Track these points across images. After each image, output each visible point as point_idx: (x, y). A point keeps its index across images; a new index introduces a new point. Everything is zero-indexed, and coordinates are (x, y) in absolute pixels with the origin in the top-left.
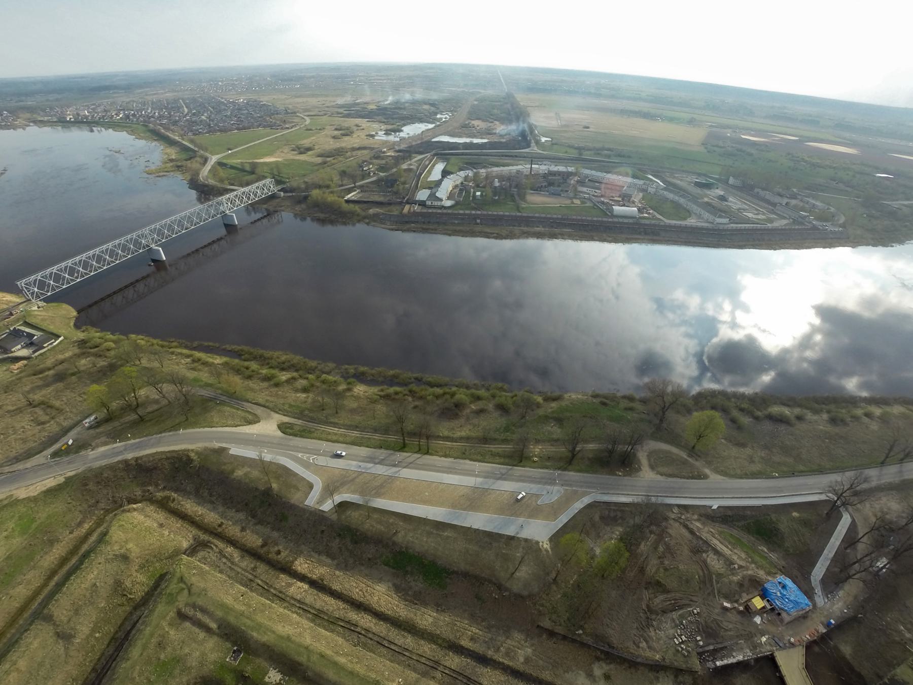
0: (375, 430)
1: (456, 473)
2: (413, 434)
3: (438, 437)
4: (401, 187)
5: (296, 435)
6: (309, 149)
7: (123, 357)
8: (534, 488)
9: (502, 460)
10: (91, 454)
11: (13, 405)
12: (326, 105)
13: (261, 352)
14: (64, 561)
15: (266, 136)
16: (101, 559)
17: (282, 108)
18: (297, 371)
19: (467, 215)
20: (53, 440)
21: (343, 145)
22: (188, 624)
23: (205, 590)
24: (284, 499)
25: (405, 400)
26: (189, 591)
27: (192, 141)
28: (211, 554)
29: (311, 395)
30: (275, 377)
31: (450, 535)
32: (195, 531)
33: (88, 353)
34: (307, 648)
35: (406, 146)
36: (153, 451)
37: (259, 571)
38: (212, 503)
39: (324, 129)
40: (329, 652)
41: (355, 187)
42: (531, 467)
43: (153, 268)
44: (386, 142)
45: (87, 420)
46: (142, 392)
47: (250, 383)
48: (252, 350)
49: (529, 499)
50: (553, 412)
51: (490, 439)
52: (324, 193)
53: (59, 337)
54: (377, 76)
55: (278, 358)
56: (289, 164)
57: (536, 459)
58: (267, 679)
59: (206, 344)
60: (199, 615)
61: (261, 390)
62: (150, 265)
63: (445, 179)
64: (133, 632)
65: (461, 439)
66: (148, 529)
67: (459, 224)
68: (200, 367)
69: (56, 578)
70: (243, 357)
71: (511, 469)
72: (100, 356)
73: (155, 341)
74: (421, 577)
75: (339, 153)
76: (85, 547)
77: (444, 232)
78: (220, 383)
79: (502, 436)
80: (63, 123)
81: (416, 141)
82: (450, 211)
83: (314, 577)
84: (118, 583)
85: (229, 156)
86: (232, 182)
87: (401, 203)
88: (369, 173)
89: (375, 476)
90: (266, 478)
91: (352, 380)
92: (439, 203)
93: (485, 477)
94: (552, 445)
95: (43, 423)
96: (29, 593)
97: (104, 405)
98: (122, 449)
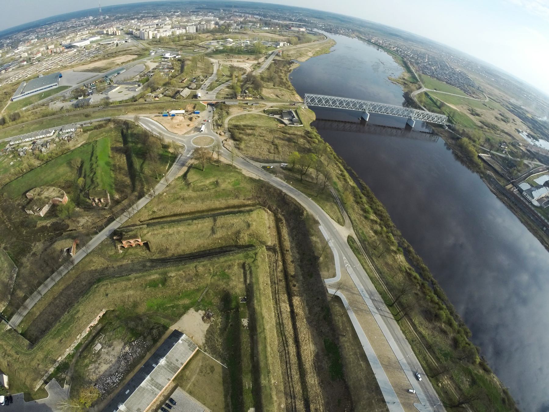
0: (387, 284)
1: (398, 345)
2: (401, 304)
3: (410, 320)
4: (515, 172)
5: (351, 248)
6: (478, 115)
7: (317, 150)
8: (422, 396)
9: (425, 366)
10: (274, 177)
11: (268, 139)
12: (503, 98)
13: (373, 196)
14: (234, 207)
15: (459, 94)
16: (243, 218)
17: (477, 85)
18: (381, 220)
19: (542, 219)
20: (268, 161)
21: (499, 125)
22: (242, 271)
23: (258, 267)
24: (319, 268)
25: (415, 285)
26: (254, 261)
27: (420, 76)
28: (273, 257)
29: (376, 237)
30: (369, 213)
31: (363, 365)
32: (277, 243)
33: (306, 138)
34: (264, 329)
35: (535, 151)
36: (293, 197)
37: (281, 283)
38: (293, 239)
39: (493, 109)
40: (268, 341)
41: (489, 152)
42: (433, 385)
43: (359, 121)
44: (525, 140)
45: (283, 164)
46: (311, 170)
47: (356, 206)
48: (370, 192)
49: (413, 397)
50: (476, 374)
51: (432, 349)
52: (470, 143)
53: (302, 124)
54: (542, 100)
55: (378, 206)
56: (462, 115)
57: (440, 385)
58: (242, 320)
59: (353, 171)
60: (248, 272)
61: (357, 213)
62: (359, 119)
63: (544, 188)
64: (228, 253)
65: (420, 333)
66: (264, 224)
67: (532, 221)
68: (341, 179)
69: (227, 210)
70: (363, 191)
71: (424, 375)
72: (309, 143)
73: (334, 153)
74: (330, 364)
75: (494, 128)
76: (242, 209)
77: (520, 217)
78: (343, 194)
79: (439, 356)
80: (369, 42)
81: (542, 152)
82: (533, 208)
83: (296, 310)
84: (239, 232)
85: (432, 92)
86: (426, 106)
87: (508, 181)
88: (503, 150)
89: (364, 303)
90: (321, 252)
91: (401, 249)
92: (530, 199)
93: (409, 364)
94: (455, 389)
95: (270, 153)
96: (218, 207)
97: (294, 163)
98: (284, 185)
